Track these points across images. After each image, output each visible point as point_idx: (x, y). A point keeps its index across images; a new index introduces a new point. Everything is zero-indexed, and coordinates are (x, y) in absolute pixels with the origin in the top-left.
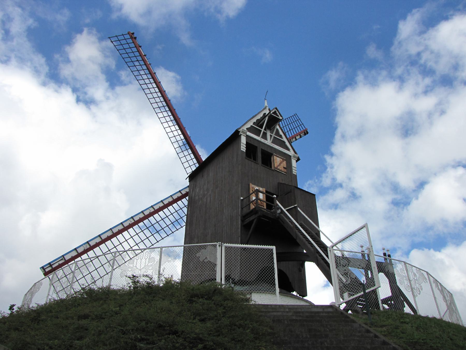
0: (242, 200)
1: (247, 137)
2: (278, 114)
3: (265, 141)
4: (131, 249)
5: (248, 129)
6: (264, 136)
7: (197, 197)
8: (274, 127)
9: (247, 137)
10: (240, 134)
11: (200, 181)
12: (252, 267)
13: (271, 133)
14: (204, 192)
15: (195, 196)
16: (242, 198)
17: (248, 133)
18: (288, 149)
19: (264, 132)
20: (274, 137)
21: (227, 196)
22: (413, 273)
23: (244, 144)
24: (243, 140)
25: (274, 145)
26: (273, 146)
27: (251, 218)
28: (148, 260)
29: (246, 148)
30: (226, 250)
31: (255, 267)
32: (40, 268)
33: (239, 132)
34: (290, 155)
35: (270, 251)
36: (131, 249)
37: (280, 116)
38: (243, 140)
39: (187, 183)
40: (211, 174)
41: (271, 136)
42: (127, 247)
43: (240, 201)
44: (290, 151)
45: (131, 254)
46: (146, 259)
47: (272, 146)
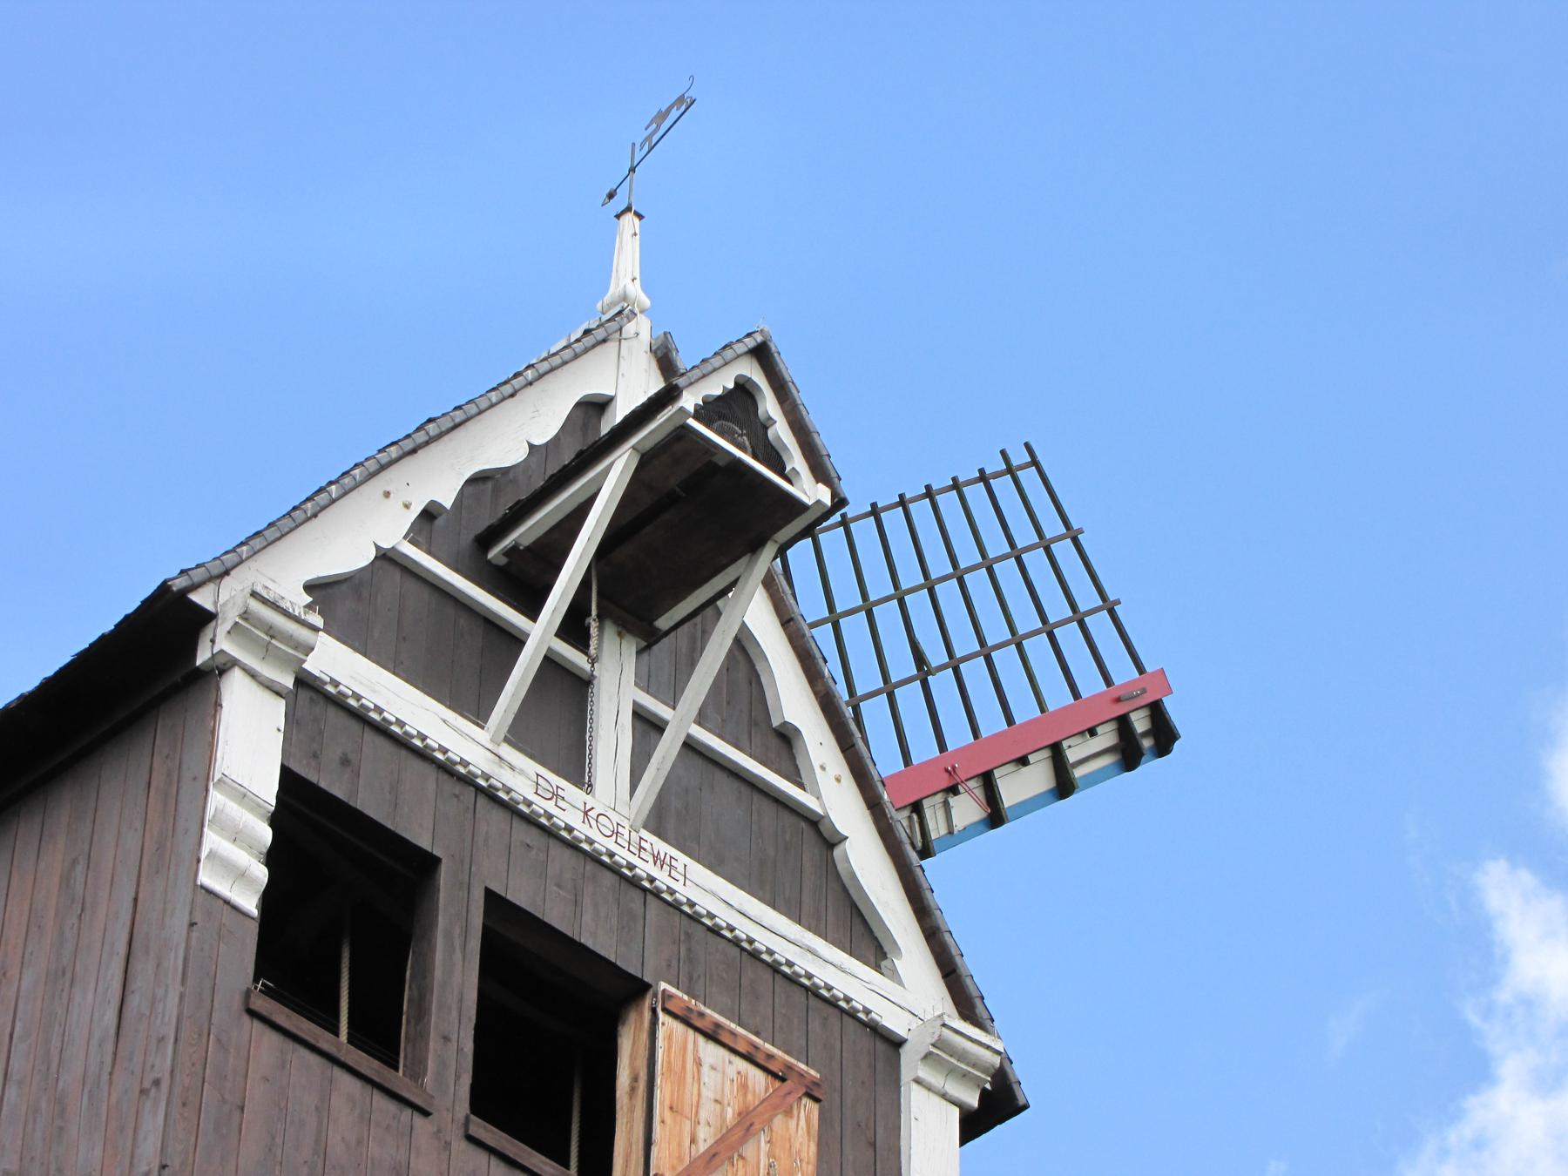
2: (781, 431)
3: (555, 796)
10: (202, 657)
13: (646, 682)
19: (551, 663)
20: (690, 746)
23: (243, 796)
26: (663, 879)
37: (796, 461)
41: (648, 726)
44: (894, 976)
47: (645, 868)
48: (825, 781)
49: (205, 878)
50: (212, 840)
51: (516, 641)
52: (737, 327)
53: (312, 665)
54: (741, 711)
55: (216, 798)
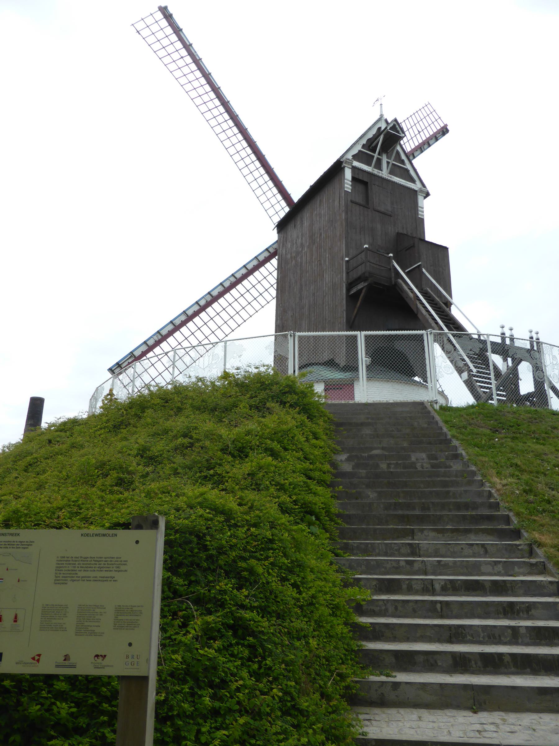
0: (347, 261)
1: (354, 169)
2: (399, 129)
3: (379, 173)
4: (200, 344)
5: (355, 157)
6: (378, 165)
7: (289, 255)
8: (394, 148)
9: (354, 169)
10: (342, 166)
11: (293, 232)
12: (376, 358)
13: (387, 158)
14: (298, 249)
15: (286, 254)
16: (347, 259)
17: (356, 164)
18: (413, 181)
19: (378, 158)
20: (393, 164)
21: (327, 256)
22: (551, 356)
23: (348, 180)
24: (348, 174)
25: (393, 176)
26: (391, 179)
27: (360, 287)
28: (211, 357)
29: (351, 186)
30: (299, 341)
31: (396, 358)
32: (108, 370)
33: (342, 162)
34: (416, 189)
35: (354, 338)
36: (200, 344)
37: (401, 132)
38: (348, 174)
39: (273, 237)
40: (306, 224)
41: (388, 163)
42: (195, 343)
43: (344, 263)
44: (416, 184)
45: (201, 349)
46: (209, 356)
47: (389, 178)
48: (407, 165)
49: (346, 189)
50: (346, 185)
51: (373, 157)
52: (393, 118)
53: (353, 165)
54: (279, 497)
55: (346, 181)
